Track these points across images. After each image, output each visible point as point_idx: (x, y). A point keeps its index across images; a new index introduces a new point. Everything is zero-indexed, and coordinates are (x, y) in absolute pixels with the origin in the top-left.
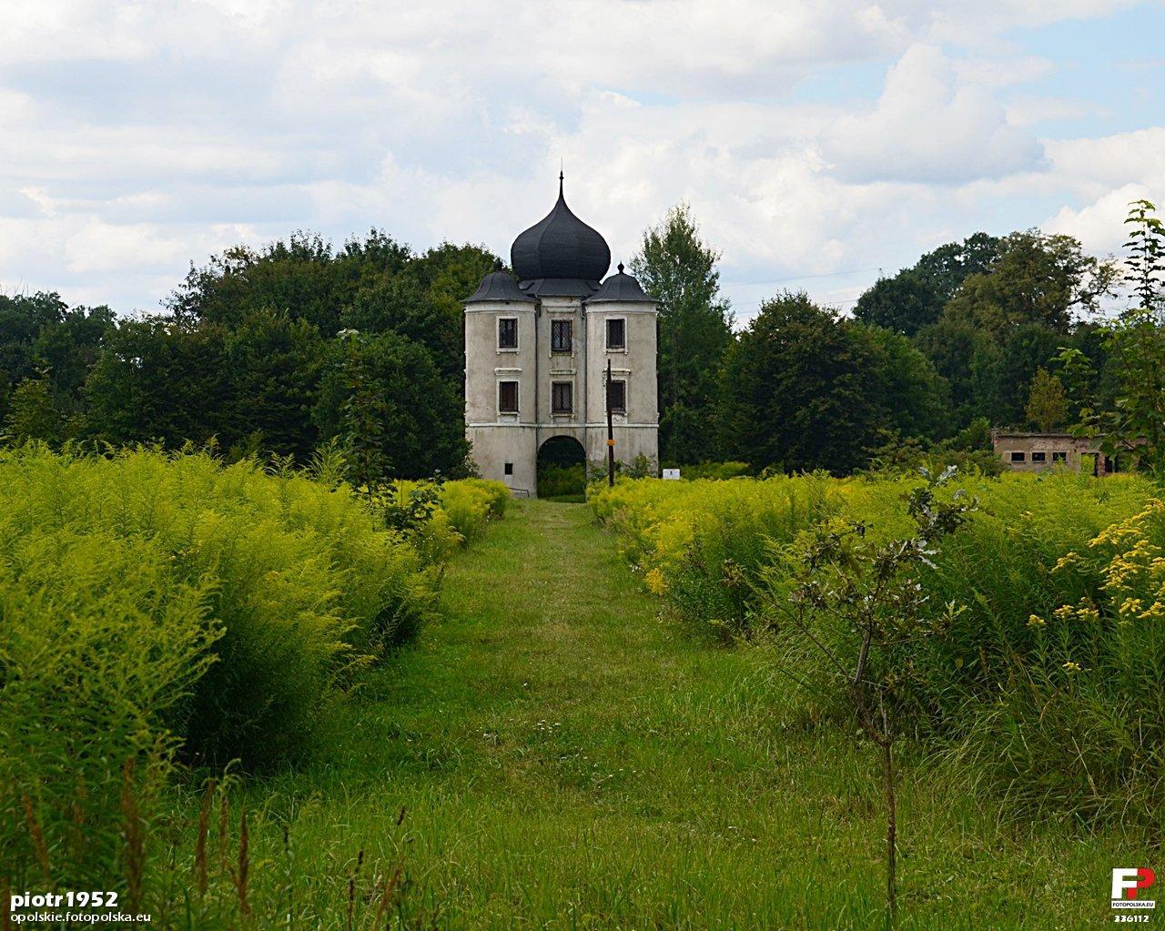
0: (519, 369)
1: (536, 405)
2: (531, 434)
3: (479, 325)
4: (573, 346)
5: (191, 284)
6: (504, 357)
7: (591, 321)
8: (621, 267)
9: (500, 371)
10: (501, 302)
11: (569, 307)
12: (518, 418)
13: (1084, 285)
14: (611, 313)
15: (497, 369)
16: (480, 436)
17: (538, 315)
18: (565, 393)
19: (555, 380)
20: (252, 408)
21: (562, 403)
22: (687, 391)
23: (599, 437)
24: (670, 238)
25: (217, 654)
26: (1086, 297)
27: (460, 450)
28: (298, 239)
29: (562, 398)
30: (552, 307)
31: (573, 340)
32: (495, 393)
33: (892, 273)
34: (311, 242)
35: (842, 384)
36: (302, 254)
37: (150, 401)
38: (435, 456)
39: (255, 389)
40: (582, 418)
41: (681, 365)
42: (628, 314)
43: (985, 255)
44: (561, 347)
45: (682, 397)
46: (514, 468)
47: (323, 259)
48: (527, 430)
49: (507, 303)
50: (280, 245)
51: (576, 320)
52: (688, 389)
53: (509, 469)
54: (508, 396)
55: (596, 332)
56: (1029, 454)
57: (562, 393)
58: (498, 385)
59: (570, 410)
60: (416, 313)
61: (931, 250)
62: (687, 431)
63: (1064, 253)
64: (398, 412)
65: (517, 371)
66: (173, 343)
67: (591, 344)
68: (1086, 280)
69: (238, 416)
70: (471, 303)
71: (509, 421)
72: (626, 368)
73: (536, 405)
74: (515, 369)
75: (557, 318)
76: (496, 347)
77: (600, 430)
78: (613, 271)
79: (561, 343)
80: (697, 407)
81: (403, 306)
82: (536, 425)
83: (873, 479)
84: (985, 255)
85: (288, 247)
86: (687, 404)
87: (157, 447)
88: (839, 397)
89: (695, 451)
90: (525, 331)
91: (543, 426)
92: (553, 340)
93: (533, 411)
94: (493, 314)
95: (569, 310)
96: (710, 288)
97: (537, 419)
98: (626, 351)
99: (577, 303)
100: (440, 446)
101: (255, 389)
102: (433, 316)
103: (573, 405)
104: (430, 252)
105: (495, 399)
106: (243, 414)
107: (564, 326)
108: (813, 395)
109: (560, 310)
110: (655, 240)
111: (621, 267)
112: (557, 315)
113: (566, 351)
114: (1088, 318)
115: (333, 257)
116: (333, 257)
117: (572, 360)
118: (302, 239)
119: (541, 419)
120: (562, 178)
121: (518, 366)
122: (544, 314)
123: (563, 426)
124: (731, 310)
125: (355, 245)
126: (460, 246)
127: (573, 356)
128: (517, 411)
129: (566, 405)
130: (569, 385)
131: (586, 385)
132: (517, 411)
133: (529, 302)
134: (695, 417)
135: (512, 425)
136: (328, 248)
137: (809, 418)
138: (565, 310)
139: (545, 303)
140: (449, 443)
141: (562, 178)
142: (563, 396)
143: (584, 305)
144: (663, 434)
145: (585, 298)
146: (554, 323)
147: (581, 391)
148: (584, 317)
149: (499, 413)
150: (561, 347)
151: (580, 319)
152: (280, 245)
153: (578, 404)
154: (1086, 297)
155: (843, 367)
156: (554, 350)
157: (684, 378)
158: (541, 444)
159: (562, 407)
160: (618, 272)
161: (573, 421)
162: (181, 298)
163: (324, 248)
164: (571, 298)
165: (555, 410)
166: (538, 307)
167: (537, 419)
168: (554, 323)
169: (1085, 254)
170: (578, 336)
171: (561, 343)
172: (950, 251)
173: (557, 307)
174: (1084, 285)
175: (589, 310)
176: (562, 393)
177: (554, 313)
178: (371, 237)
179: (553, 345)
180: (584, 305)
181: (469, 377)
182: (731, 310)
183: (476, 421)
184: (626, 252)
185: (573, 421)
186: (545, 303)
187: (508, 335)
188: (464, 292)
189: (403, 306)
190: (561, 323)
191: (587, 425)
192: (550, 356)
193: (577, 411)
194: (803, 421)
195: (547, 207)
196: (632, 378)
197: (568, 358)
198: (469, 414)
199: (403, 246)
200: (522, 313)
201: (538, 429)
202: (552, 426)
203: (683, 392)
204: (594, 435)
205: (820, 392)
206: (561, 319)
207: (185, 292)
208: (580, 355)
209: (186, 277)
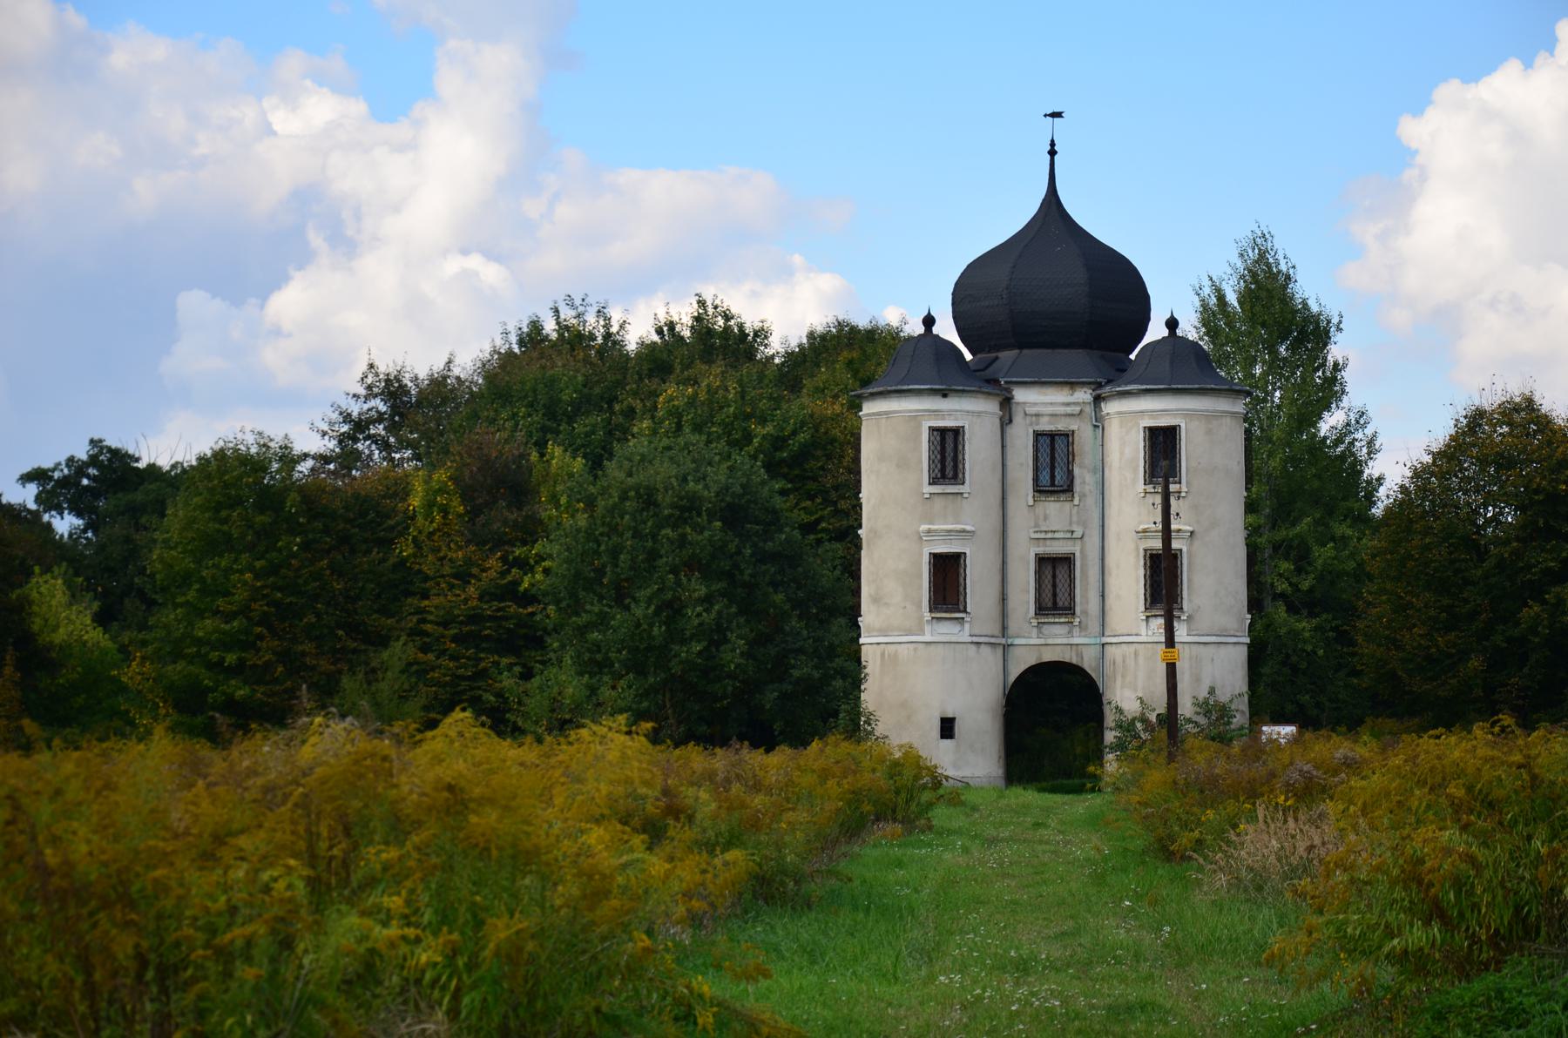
0: (968, 528)
1: (1003, 599)
2: (989, 660)
4: (1077, 482)
6: (939, 503)
7: (1114, 429)
8: (1172, 324)
9: (929, 531)
10: (933, 392)
11: (1068, 404)
12: (967, 626)
15: (924, 527)
16: (890, 661)
17: (1006, 421)
19: (1041, 550)
20: (456, 612)
21: (1055, 595)
22: (1291, 584)
23: (1131, 662)
27: (838, 683)
28: (567, 314)
29: (1054, 586)
30: (1036, 404)
31: (1077, 471)
32: (920, 576)
34: (591, 319)
37: (265, 596)
40: (1094, 626)
41: (1282, 534)
44: (1053, 484)
45: (1282, 596)
46: (958, 728)
48: (985, 650)
49: (945, 396)
50: (536, 326)
51: (1084, 433)
52: (1294, 580)
53: (947, 728)
55: (1122, 453)
57: (1054, 577)
58: (926, 559)
59: (1069, 610)
60: (769, 429)
62: (1294, 659)
64: (708, 600)
65: (964, 531)
67: (1114, 477)
69: (428, 627)
70: (874, 396)
71: (947, 631)
72: (1185, 524)
73: (1003, 599)
74: (959, 527)
75: (1046, 425)
76: (921, 485)
77: (1132, 648)
78: (1156, 331)
79: (1053, 477)
80: (1312, 615)
81: (748, 417)
82: (1003, 641)
83: (853, 792)
85: (550, 327)
86: (1292, 609)
89: (1307, 697)
90: (978, 452)
91: (1017, 641)
92: (1036, 470)
94: (915, 418)
95: (1069, 410)
96: (1330, 391)
97: (1004, 628)
98: (1184, 489)
99: (1084, 395)
100: (796, 673)
103: (1078, 599)
104: (811, 335)
105: (920, 587)
106: (438, 624)
107: (1059, 442)
109: (1050, 410)
111: (1172, 324)
112: (1045, 420)
113: (1063, 491)
115: (632, 346)
116: (632, 346)
117: (1075, 510)
118: (574, 313)
120: (1052, 153)
122: (1018, 419)
124: (1369, 431)
125: (671, 325)
127: (1076, 501)
128: (965, 611)
129: (1062, 600)
130: (1067, 561)
131: (1103, 559)
132: (965, 611)
133: (989, 394)
134: (1307, 634)
135: (954, 639)
136: (622, 327)
137: (1545, 622)
138: (1062, 410)
139: (1021, 395)
140: (816, 667)
141: (1052, 153)
143: (1098, 400)
145: (1099, 386)
148: (1099, 423)
149: (927, 616)
150: (1053, 484)
151: (1090, 428)
152: (536, 326)
153: (1087, 598)
156: (1039, 490)
157: (1287, 558)
158: (1012, 678)
159: (1055, 603)
160: (1165, 332)
161: (1076, 631)
162: (347, 417)
163: (614, 329)
164: (1072, 385)
165: (1041, 609)
166: (1007, 403)
167: (1004, 628)
170: (1087, 462)
171: (1053, 477)
175: (1111, 407)
176: (1054, 577)
177: (1037, 415)
179: (1036, 480)
180: (1098, 400)
181: (868, 545)
182: (1369, 431)
185: (1076, 631)
186: (1021, 395)
189: (748, 417)
190: (1052, 436)
191: (1105, 640)
192: (1031, 502)
193: (1085, 612)
196: (1197, 543)
197: (1067, 505)
198: (869, 617)
199: (757, 325)
201: (1006, 648)
202: (1032, 642)
203: (1285, 586)
204: (1119, 660)
206: (1052, 428)
208: (1091, 502)
209: (359, 379)
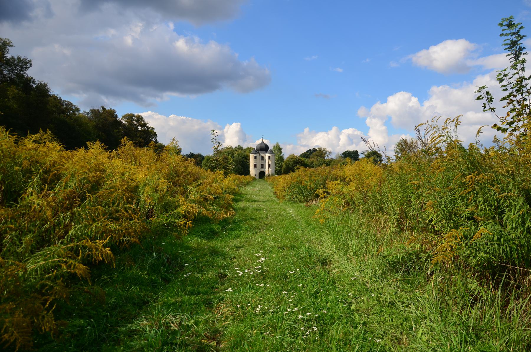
3: (252, 156)
24: (276, 146)
25: (291, 171)
26: (327, 156)
33: (55, 90)
47: (232, 148)
54: (255, 166)
63: (325, 150)
68: (327, 153)
78: (269, 150)
87: (117, 181)
90: (258, 157)
114: (328, 158)
123: (262, 170)
154: (327, 156)
172: (310, 150)
173: (262, 154)
184: (271, 147)
187: (255, 158)
188: (250, 152)
198: (250, 168)
200: (257, 155)
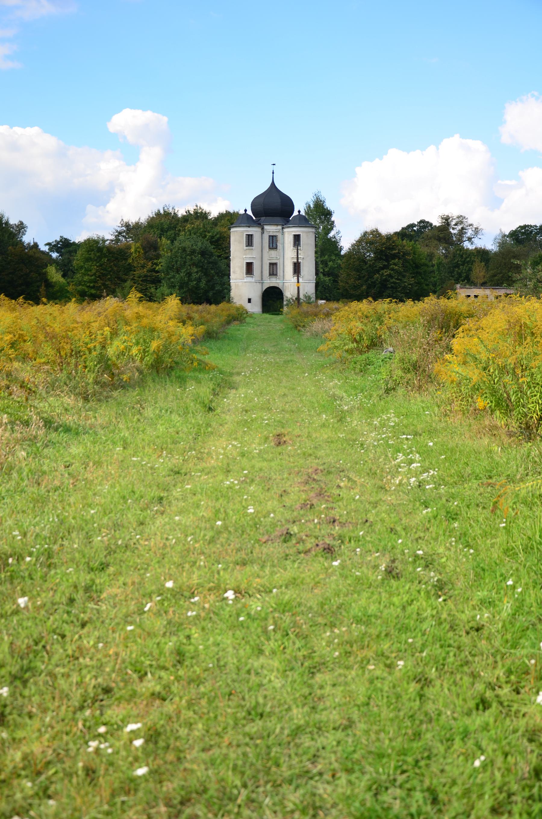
1: (262, 272)
2: (259, 285)
5: (122, 226)
6: (248, 251)
7: (286, 235)
8: (299, 212)
13: (468, 235)
14: (295, 231)
17: (263, 233)
18: (275, 266)
26: (470, 239)
35: (395, 264)
36: (167, 214)
38: (214, 294)
39: (143, 267)
40: (282, 279)
42: (303, 232)
43: (424, 227)
53: (249, 301)
54: (249, 267)
56: (472, 295)
59: (276, 275)
61: (405, 225)
64: (197, 272)
66: (109, 249)
67: (286, 246)
71: (249, 279)
73: (262, 272)
75: (271, 234)
78: (296, 213)
84: (424, 227)
88: (393, 270)
90: (256, 240)
93: (260, 275)
94: (242, 232)
101: (143, 267)
102: (218, 236)
107: (274, 238)
108: (383, 268)
110: (309, 207)
111: (299, 212)
119: (264, 278)
121: (252, 255)
122: (265, 232)
126: (232, 212)
129: (275, 273)
130: (276, 264)
139: (266, 227)
142: (273, 269)
144: (317, 285)
146: (270, 236)
147: (282, 267)
148: (283, 233)
153: (280, 272)
154: (470, 239)
155: (394, 256)
156: (270, 248)
162: (117, 231)
164: (277, 225)
165: (270, 275)
168: (270, 236)
169: (470, 222)
173: (271, 229)
174: (468, 235)
175: (285, 230)
178: (195, 208)
180: (283, 228)
183: (236, 279)
186: (266, 227)
190: (273, 236)
194: (377, 280)
195: (266, 186)
198: (232, 276)
200: (255, 231)
205: (385, 267)
207: (119, 229)
208: (281, 251)
